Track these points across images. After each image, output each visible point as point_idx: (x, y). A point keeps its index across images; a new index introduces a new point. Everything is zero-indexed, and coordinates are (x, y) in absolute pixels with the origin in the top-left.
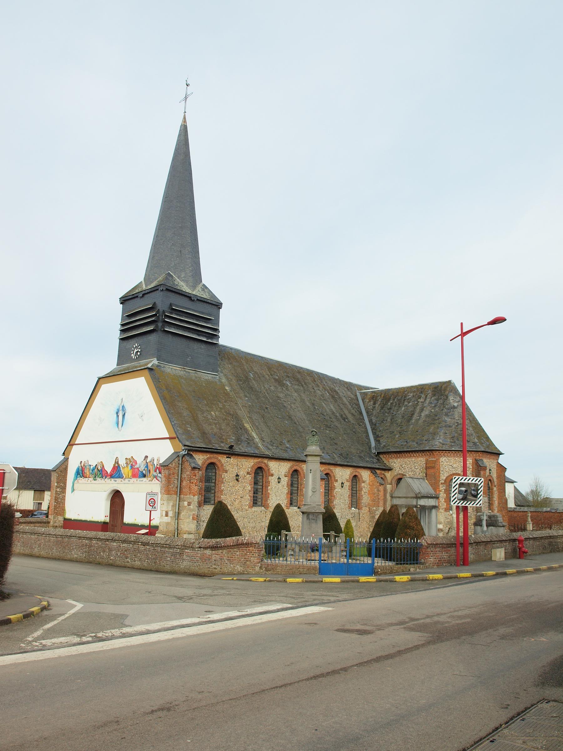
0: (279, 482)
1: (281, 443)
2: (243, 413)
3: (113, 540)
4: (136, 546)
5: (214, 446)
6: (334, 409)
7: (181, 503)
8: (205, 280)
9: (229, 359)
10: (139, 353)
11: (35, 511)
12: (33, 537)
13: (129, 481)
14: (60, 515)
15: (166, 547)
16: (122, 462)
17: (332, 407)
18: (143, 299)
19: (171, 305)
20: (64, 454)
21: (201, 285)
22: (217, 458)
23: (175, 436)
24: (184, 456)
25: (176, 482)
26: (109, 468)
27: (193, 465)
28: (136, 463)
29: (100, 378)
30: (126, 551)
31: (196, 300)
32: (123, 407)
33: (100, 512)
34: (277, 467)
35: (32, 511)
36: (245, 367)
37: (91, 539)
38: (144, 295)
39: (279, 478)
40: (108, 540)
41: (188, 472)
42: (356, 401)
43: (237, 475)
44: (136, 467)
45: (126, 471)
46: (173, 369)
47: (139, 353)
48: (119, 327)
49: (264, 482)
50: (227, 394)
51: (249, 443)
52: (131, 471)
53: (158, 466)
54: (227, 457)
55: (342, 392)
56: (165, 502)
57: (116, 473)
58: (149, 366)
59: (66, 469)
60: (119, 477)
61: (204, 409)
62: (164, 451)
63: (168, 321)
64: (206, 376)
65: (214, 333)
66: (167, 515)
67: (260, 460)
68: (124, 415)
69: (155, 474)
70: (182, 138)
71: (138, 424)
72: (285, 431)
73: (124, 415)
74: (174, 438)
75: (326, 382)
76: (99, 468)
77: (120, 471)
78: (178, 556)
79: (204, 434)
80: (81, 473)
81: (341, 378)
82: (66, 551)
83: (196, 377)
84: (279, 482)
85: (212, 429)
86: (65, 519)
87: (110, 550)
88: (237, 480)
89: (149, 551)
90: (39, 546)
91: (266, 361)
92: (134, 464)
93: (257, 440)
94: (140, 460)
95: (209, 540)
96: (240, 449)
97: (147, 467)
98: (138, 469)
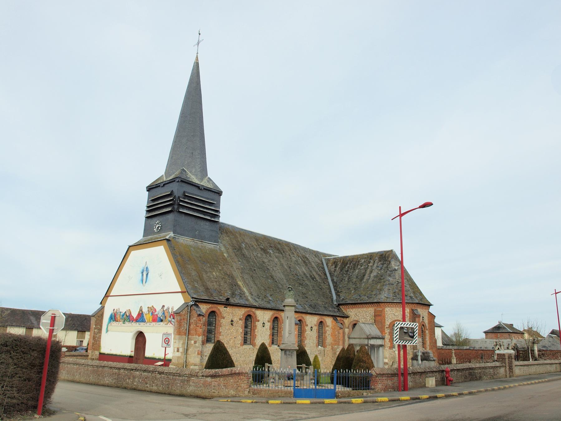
2: (237, 274)
3: (136, 370)
4: (153, 375)
7: (189, 342)
9: (227, 233)
12: (75, 366)
14: (97, 350)
16: (145, 310)
19: (184, 192)
20: (101, 303)
21: (207, 178)
22: (217, 308)
24: (192, 305)
25: (185, 325)
26: (135, 315)
28: (156, 311)
29: (130, 246)
30: (146, 378)
32: (147, 268)
37: (119, 369)
39: (264, 323)
40: (132, 370)
41: (194, 318)
42: (321, 265)
43: (232, 321)
46: (185, 240)
48: (145, 208)
50: (225, 259)
55: (311, 258)
56: (177, 341)
57: (140, 318)
58: (167, 237)
63: (181, 205)
64: (209, 246)
65: (216, 214)
66: (178, 351)
67: (249, 309)
68: (147, 275)
69: (170, 319)
70: (195, 71)
71: (158, 282)
73: (147, 275)
76: (128, 314)
77: (143, 316)
78: (186, 383)
79: (207, 289)
80: (114, 318)
81: (311, 248)
86: (100, 354)
87: (134, 377)
90: (80, 373)
93: (247, 294)
94: (158, 308)
95: (210, 370)
98: (157, 315)
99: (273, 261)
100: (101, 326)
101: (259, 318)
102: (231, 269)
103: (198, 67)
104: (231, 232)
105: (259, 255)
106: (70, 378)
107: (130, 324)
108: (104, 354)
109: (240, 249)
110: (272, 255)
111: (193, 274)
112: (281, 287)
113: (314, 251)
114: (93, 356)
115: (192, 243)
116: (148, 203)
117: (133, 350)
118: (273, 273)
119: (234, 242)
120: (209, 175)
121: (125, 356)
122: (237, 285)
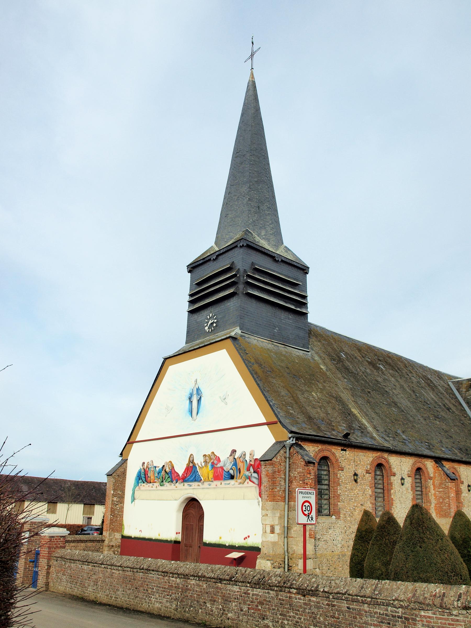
0: (403, 484)
1: (397, 434)
2: (346, 396)
3: (231, 580)
4: (283, 595)
5: (326, 434)
6: (433, 397)
8: (286, 242)
9: (316, 337)
10: (215, 325)
11: (85, 526)
12: (85, 567)
13: (210, 485)
14: (118, 531)
15: (363, 602)
16: (199, 461)
17: (432, 396)
18: (218, 261)
19: (253, 264)
20: (121, 454)
21: (282, 247)
22: (330, 451)
23: (275, 419)
24: (292, 445)
25: (282, 483)
26: (180, 470)
27: (307, 458)
28: (219, 460)
29: (166, 359)
30: (261, 603)
31: (280, 260)
32: (198, 389)
33: (167, 526)
34: (398, 464)
35: (81, 526)
36: (335, 347)
37: (186, 576)
38: (218, 256)
39: (402, 479)
40: (221, 580)
41: (300, 468)
42: (451, 391)
43: (355, 475)
44: (219, 465)
45: (205, 472)
46: (258, 342)
47: (215, 325)
48: (188, 298)
49: (385, 484)
50: (324, 374)
51: (362, 432)
52: (213, 471)
53: (252, 463)
54: (342, 450)
55: (436, 381)
56: (269, 513)
57: (191, 475)
58: (233, 334)
59: (124, 473)
60: (195, 481)
61: (304, 389)
62: (261, 441)
63: (246, 286)
64: (297, 353)
66: (272, 531)
67: (379, 454)
68: (199, 401)
69: (248, 473)
70: (251, 92)
71: (222, 406)
72: (396, 420)
73: (199, 401)
74: (275, 423)
75: (417, 369)
76: (168, 470)
77: (196, 472)
79: (310, 418)
80: (143, 477)
81: (429, 366)
82: (141, 595)
83: (287, 352)
84: (403, 484)
85: (317, 413)
86: (123, 537)
87: (226, 600)
88: (356, 481)
89: (318, 608)
90: (96, 583)
91: (353, 342)
92: (215, 462)
93: (370, 429)
94: (224, 456)
96: (357, 440)
97: (235, 464)
98: (222, 468)
99: (390, 381)
100: (123, 491)
101: (395, 470)
102: (336, 389)
103: (255, 87)
104: (320, 335)
105: (368, 371)
106: (77, 591)
107: (172, 486)
108: (130, 538)
109: (340, 360)
110: (386, 372)
111: (283, 393)
112: (411, 419)
113: (436, 371)
114: (111, 540)
115: (270, 346)
116: (191, 290)
117: (180, 531)
118: (396, 399)
119: (329, 349)
120: (285, 244)
121: (167, 541)
122: (350, 413)
